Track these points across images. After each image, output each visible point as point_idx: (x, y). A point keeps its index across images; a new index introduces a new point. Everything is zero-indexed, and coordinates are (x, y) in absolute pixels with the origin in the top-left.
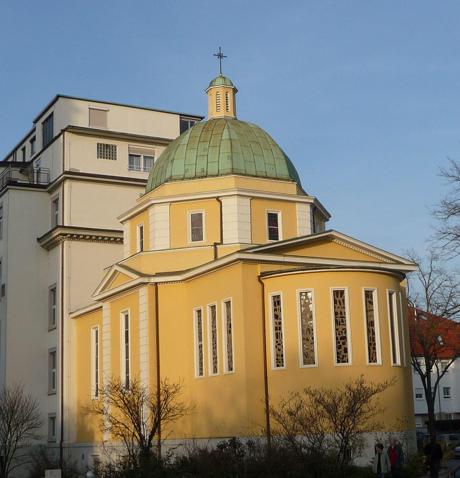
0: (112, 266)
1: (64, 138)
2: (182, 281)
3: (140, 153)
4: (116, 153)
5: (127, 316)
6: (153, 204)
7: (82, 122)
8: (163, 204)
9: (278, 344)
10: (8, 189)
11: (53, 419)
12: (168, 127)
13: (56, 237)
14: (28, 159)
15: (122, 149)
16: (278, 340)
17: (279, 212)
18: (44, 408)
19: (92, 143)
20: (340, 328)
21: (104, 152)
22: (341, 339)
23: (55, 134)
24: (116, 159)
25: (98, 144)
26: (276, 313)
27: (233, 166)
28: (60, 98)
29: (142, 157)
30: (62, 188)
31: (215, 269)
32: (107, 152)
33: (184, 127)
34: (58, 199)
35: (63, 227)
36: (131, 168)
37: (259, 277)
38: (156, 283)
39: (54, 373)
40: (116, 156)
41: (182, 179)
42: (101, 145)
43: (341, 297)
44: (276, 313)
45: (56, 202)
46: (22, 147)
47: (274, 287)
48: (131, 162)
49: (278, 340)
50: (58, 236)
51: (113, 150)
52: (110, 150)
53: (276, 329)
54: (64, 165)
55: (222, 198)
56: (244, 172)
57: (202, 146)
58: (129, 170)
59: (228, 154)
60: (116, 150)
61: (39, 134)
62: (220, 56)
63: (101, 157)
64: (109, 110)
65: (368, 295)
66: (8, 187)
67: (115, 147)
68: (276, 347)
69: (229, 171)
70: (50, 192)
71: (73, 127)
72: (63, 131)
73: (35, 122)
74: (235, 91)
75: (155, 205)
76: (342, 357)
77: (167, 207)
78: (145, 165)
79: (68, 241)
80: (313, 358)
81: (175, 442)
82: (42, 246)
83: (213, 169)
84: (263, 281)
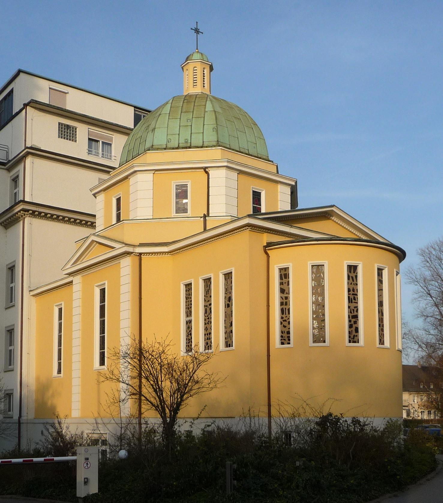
0: (87, 237)
1: (26, 112)
2: (168, 252)
3: (100, 138)
4: (76, 135)
5: (103, 291)
6: (135, 172)
7: (44, 98)
8: (146, 172)
9: (284, 321)
12: (124, 116)
13: (17, 213)
17: (263, 190)
19: (53, 122)
20: (353, 305)
21: (65, 132)
22: (353, 317)
23: (15, 110)
24: (76, 141)
25: (59, 124)
26: (282, 286)
27: (218, 138)
28: (21, 74)
29: (101, 142)
30: (23, 164)
31: (192, 245)
32: (67, 133)
33: (137, 119)
34: (18, 176)
35: (24, 201)
36: (90, 152)
37: (265, 247)
38: (140, 254)
40: (76, 138)
41: (165, 149)
42: (62, 125)
43: (354, 272)
44: (282, 286)
45: (15, 180)
47: (280, 258)
48: (90, 146)
49: (284, 316)
50: (19, 211)
51: (73, 131)
52: (70, 131)
53: (282, 304)
54: (25, 141)
55: (210, 169)
56: (228, 146)
57: (185, 117)
58: (89, 154)
59: (212, 126)
60: (76, 132)
62: (197, 31)
63: (62, 138)
64: (68, 93)
65: (380, 271)
67: (76, 129)
69: (215, 143)
70: (9, 170)
71: (36, 101)
72: (26, 105)
74: (211, 69)
75: (138, 173)
76: (353, 338)
77: (150, 176)
78: (103, 151)
79: (30, 218)
80: (324, 337)
83: (197, 140)
84: (269, 252)
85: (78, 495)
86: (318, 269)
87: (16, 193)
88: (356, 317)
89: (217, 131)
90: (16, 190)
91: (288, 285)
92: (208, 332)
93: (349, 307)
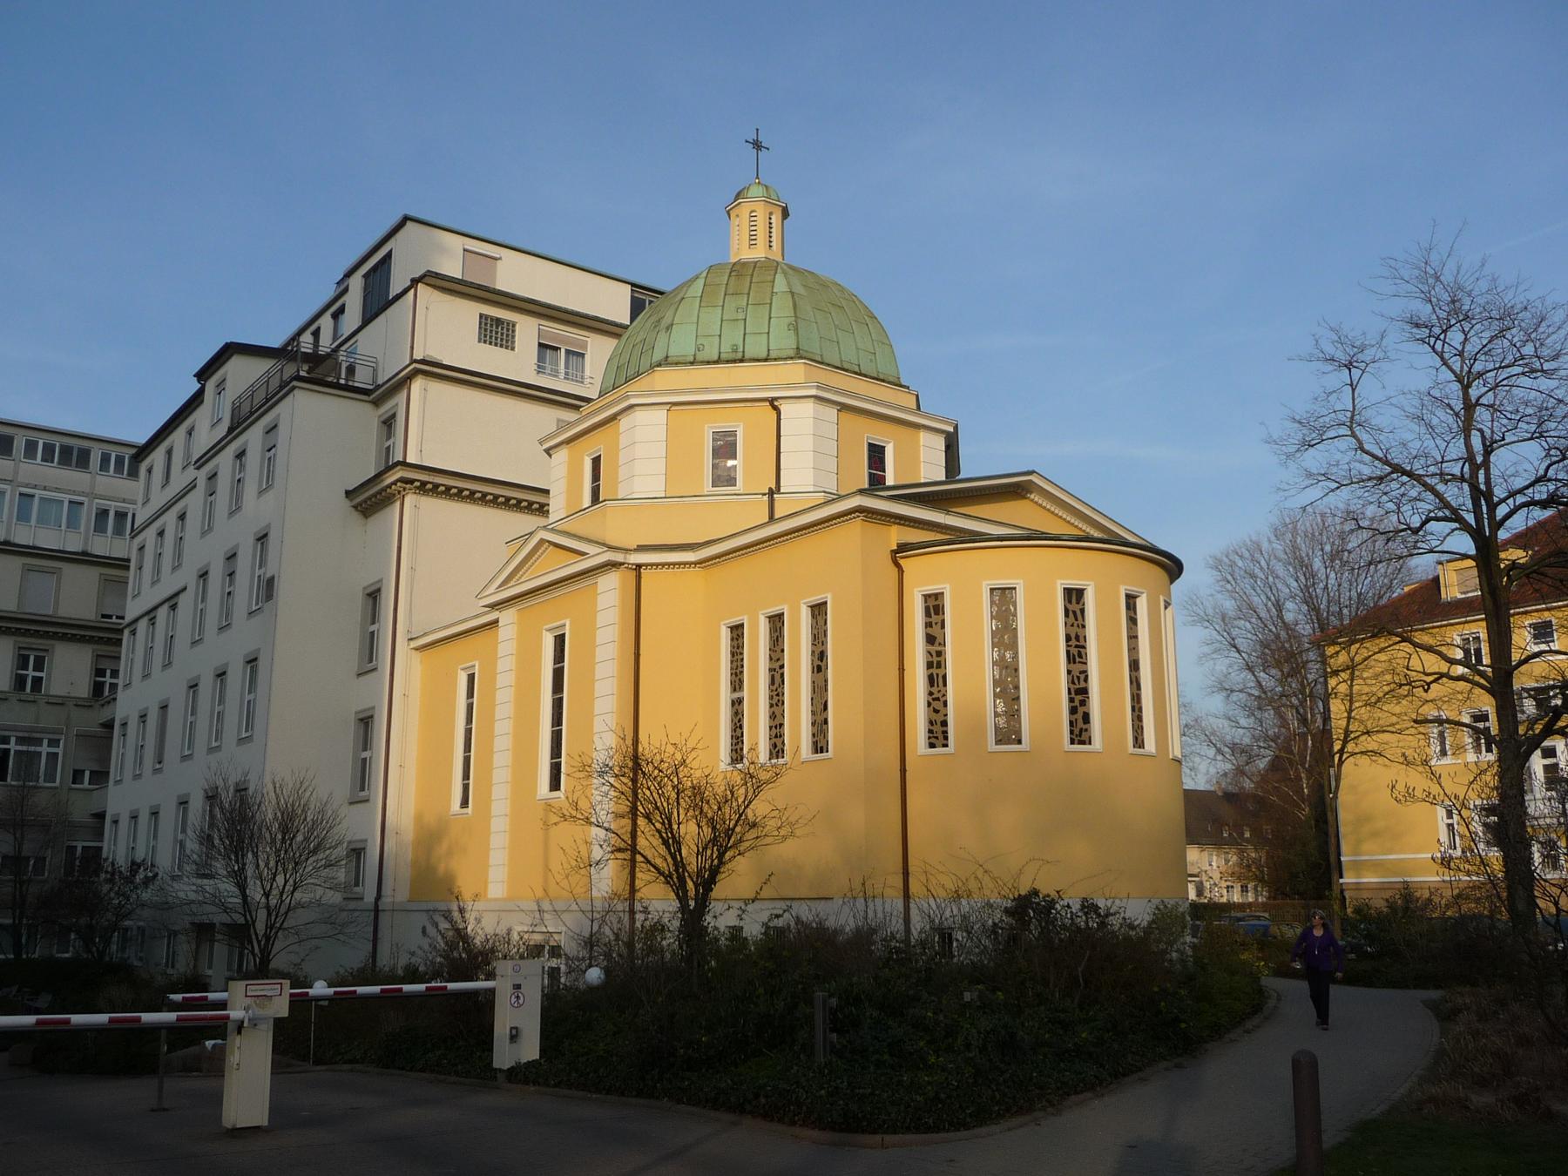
2: (696, 563)
6: (631, 407)
10: (294, 388)
11: (357, 853)
12: (613, 303)
13: (389, 486)
14: (323, 350)
15: (527, 330)
16: (934, 690)
18: (352, 825)
19: (470, 312)
20: (1076, 668)
22: (1079, 693)
23: (395, 289)
25: (481, 316)
26: (930, 631)
28: (409, 224)
33: (637, 308)
34: (394, 415)
35: (404, 464)
36: (540, 369)
37: (895, 552)
38: (639, 566)
39: (364, 760)
41: (692, 363)
44: (930, 631)
45: (388, 423)
46: (313, 328)
47: (925, 574)
48: (541, 358)
49: (934, 690)
50: (395, 483)
53: (930, 665)
57: (731, 303)
59: (787, 321)
61: (354, 302)
62: (757, 145)
65: (1131, 600)
66: (295, 383)
68: (929, 704)
70: (377, 403)
72: (415, 282)
73: (348, 275)
74: (785, 213)
76: (1080, 734)
77: (660, 415)
78: (567, 367)
80: (1018, 732)
81: (740, 906)
82: (355, 507)
83: (755, 347)
84: (901, 562)
85: (496, 1065)
86: (1003, 597)
87: (388, 448)
88: (1084, 691)
89: (796, 330)
90: (390, 442)
91: (943, 627)
92: (777, 722)
93: (1069, 672)
